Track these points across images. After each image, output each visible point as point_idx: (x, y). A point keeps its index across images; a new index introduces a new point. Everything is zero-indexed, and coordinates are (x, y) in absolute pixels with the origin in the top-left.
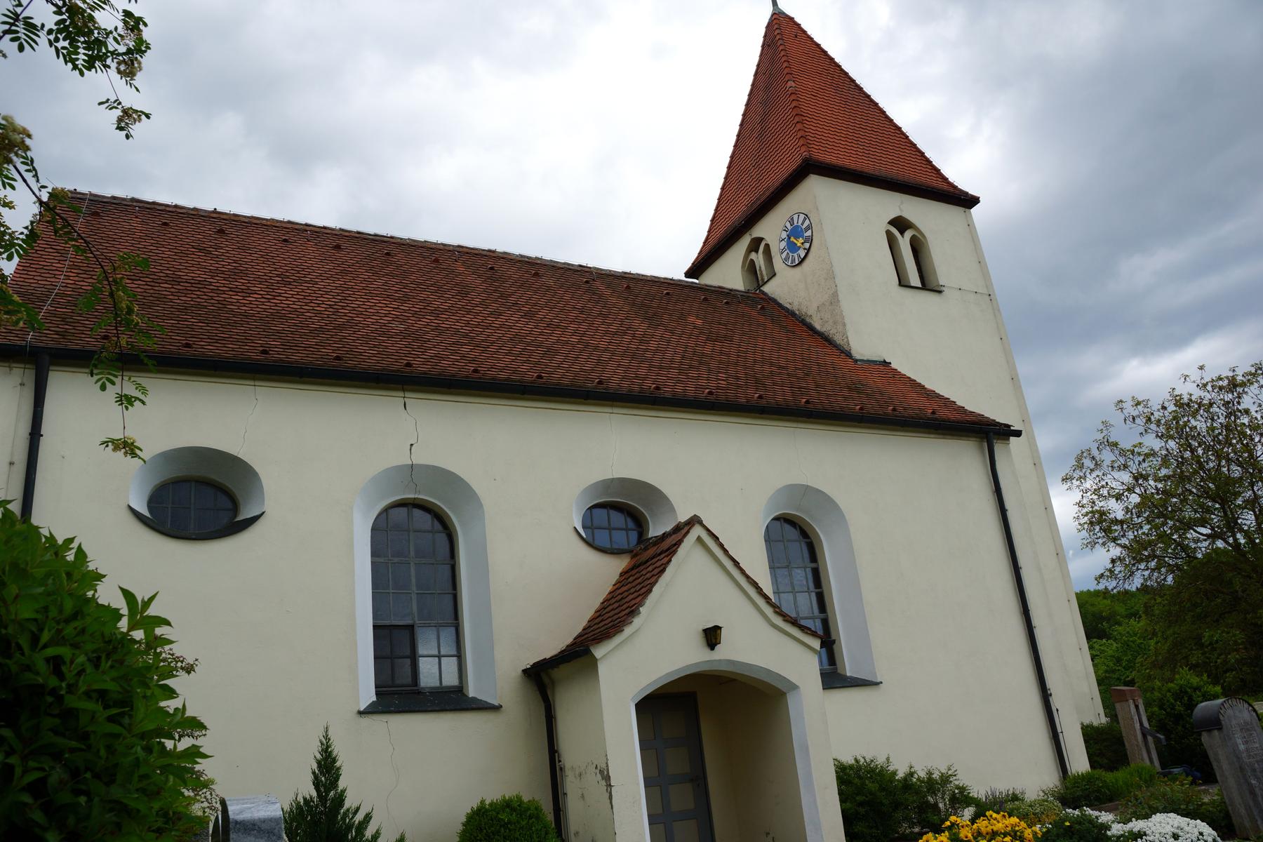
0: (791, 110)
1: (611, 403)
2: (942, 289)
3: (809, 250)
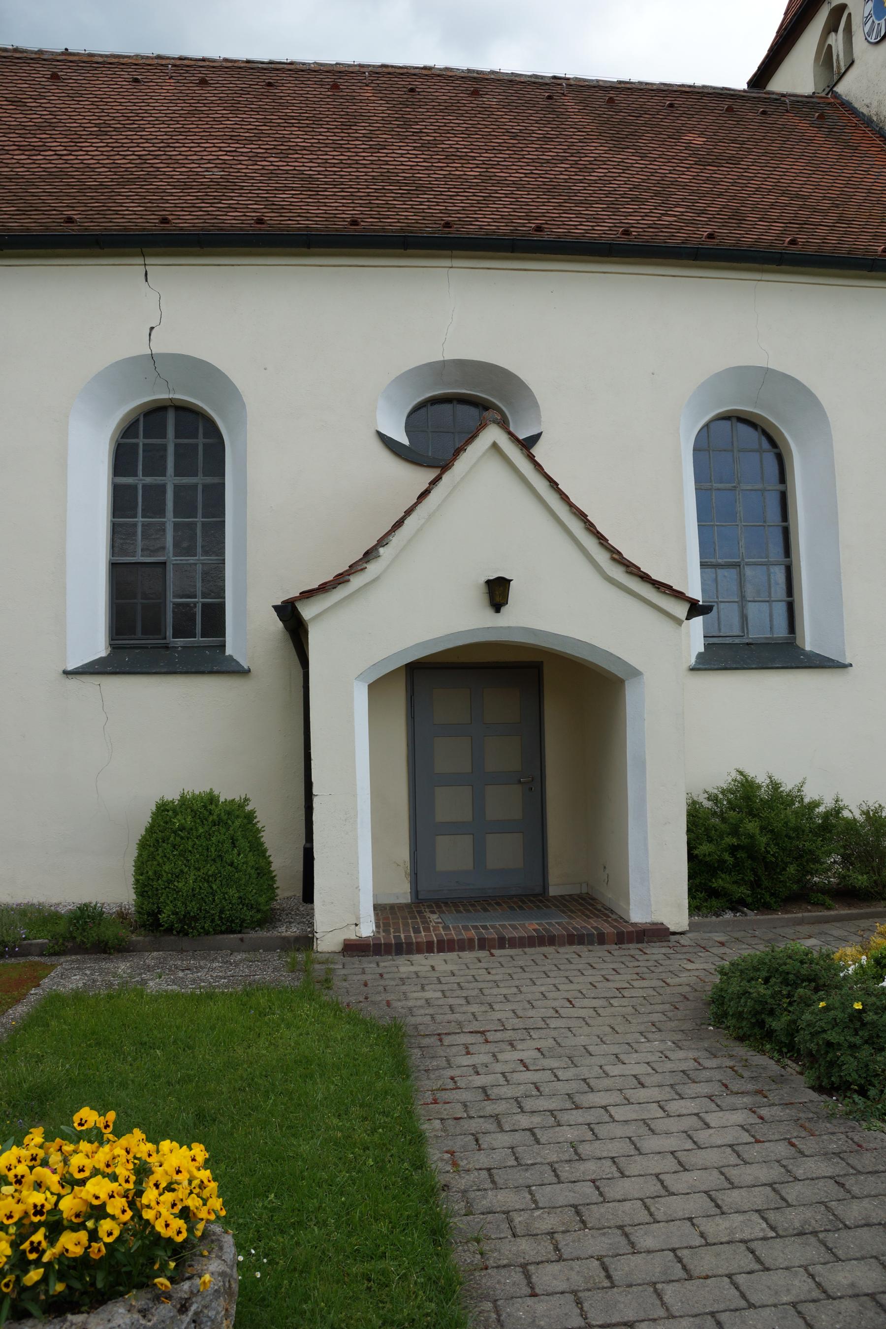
1: (449, 252)
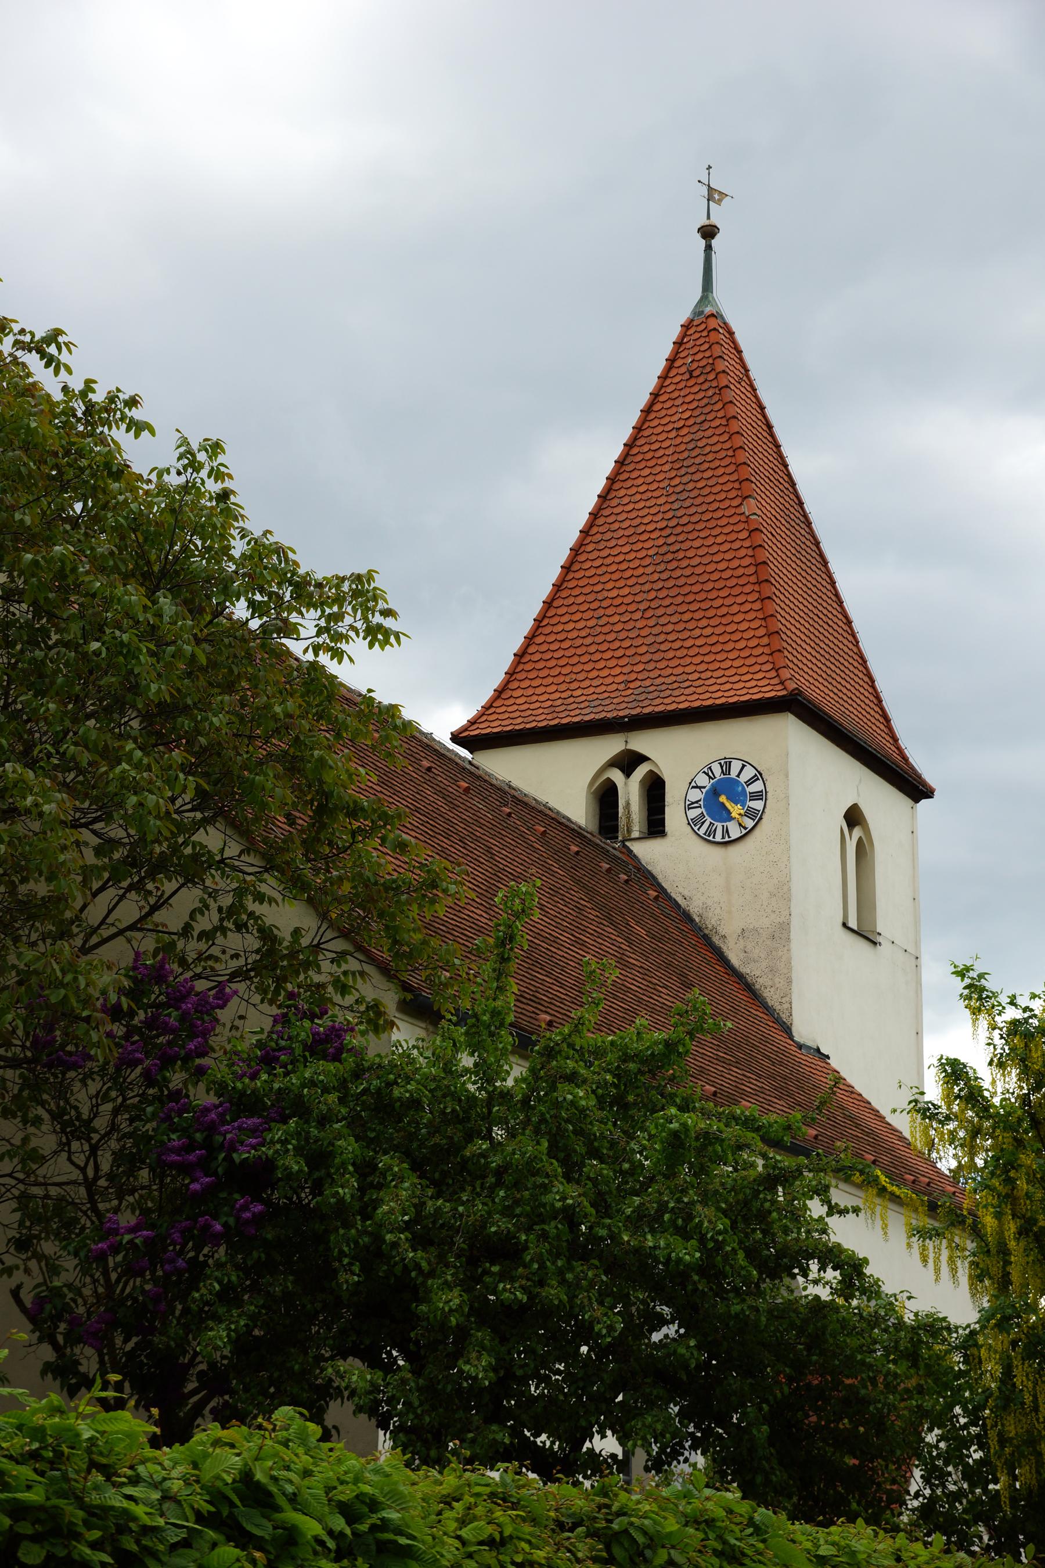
2: (879, 939)
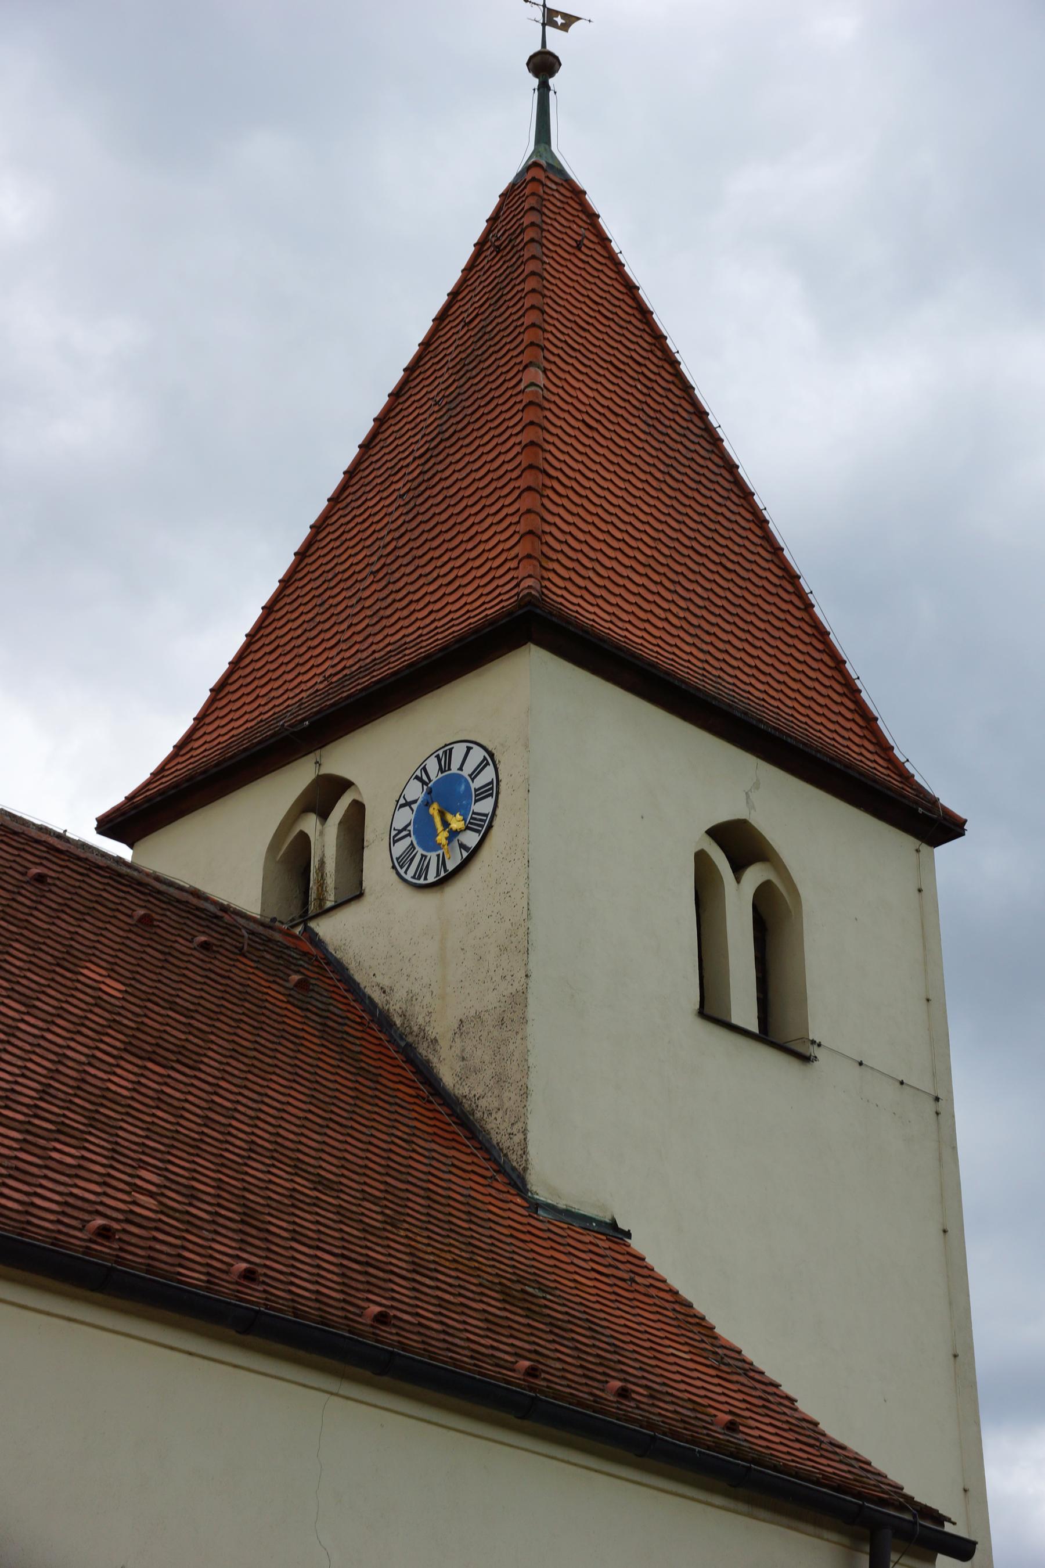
0: (517, 449)
3: (474, 853)
